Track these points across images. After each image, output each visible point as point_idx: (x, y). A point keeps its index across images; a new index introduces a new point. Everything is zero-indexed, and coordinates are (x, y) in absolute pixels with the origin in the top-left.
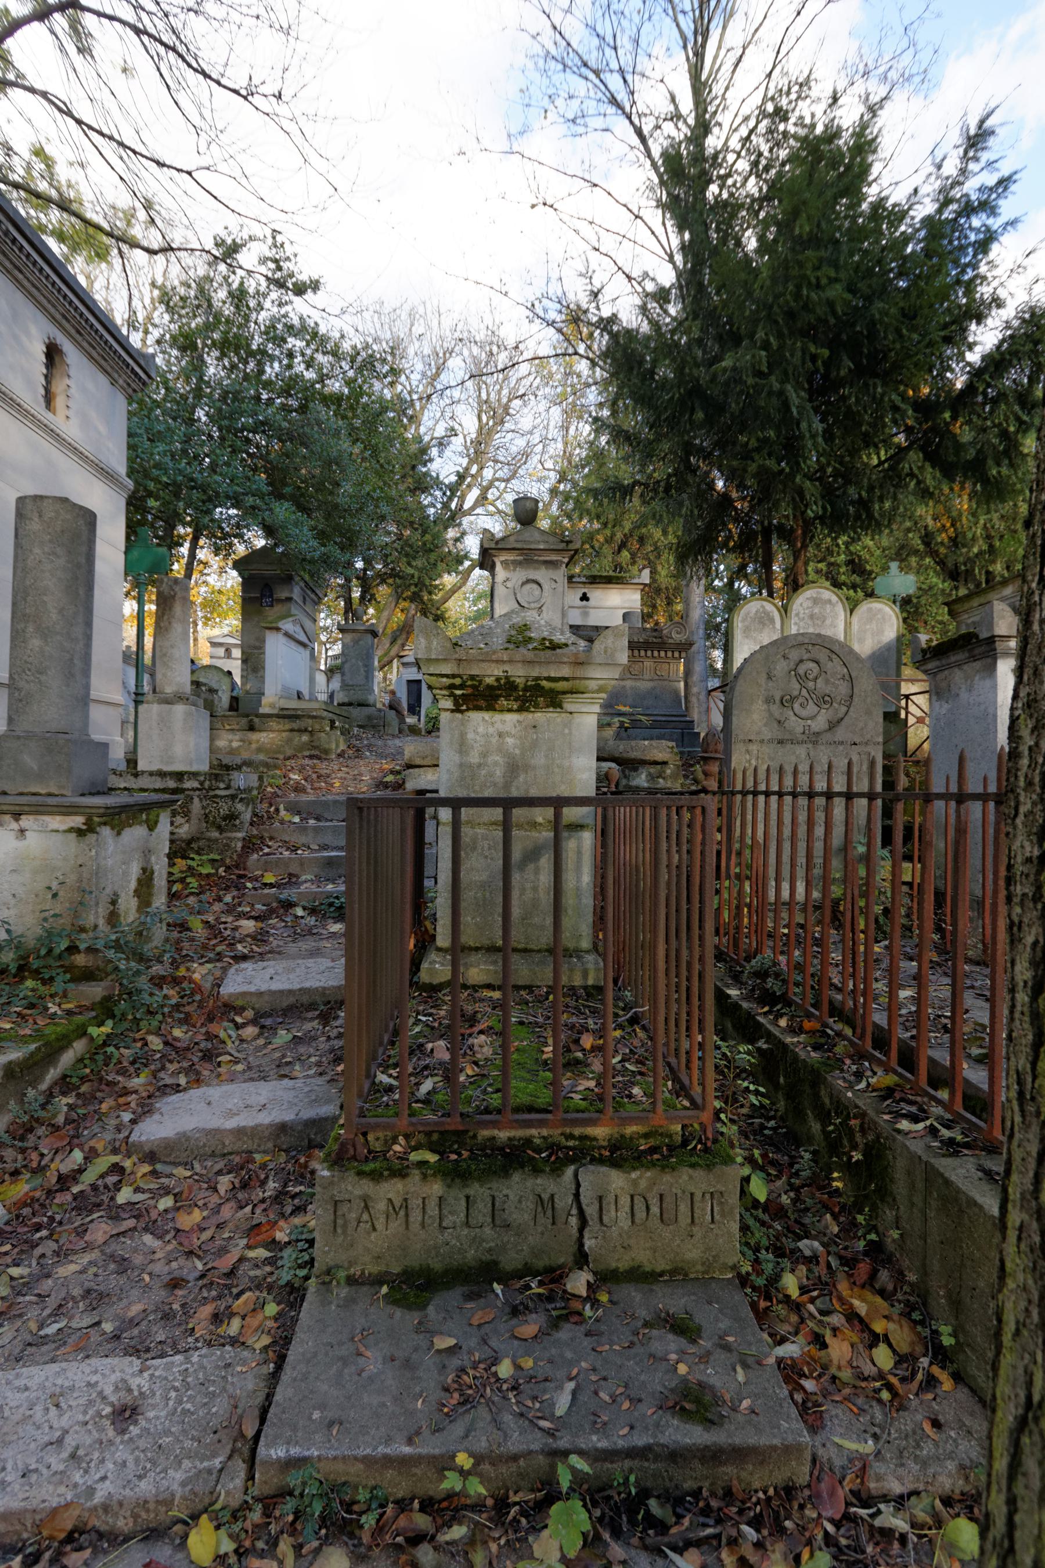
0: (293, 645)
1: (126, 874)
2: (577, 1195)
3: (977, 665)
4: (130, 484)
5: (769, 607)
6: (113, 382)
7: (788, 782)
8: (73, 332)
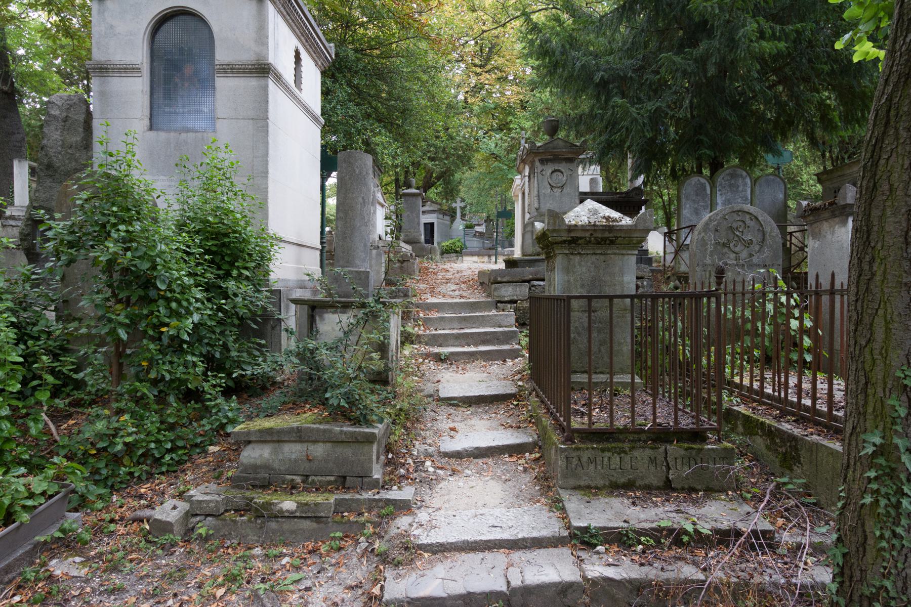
2: (666, 458)
3: (837, 220)
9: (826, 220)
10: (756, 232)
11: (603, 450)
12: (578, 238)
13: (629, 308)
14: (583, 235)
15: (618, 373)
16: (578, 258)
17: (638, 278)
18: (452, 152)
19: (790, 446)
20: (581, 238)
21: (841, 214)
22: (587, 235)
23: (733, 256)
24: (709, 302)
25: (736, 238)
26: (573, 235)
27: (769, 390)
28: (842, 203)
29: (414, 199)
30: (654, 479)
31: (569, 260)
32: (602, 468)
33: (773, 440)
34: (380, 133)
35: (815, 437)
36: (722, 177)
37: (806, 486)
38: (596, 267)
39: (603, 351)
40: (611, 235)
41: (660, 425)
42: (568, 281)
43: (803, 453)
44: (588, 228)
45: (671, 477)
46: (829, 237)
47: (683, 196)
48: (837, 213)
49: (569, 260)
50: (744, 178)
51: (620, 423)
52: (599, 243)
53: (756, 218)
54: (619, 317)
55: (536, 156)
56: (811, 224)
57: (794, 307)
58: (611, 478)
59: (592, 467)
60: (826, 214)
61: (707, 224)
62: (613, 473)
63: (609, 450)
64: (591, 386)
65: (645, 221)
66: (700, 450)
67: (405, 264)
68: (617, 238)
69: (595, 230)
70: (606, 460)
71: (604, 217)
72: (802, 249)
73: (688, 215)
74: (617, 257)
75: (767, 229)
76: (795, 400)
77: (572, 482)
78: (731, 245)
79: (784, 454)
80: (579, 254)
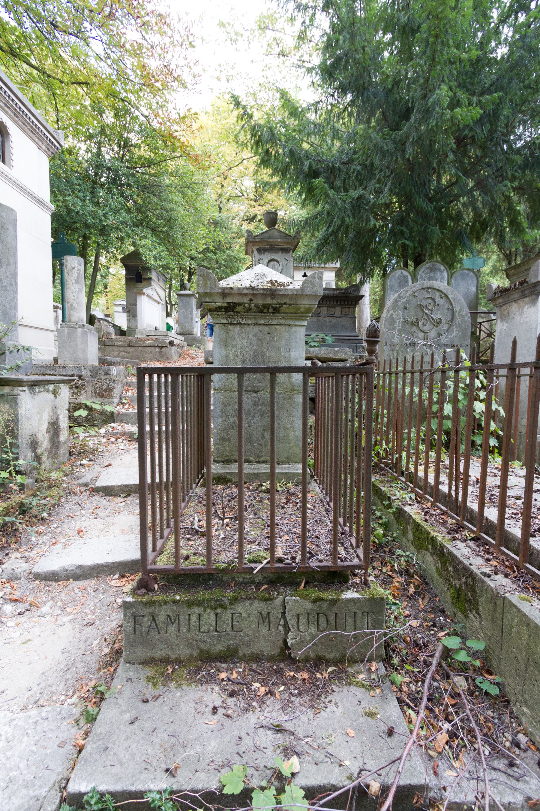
0: (152, 302)
1: (40, 419)
2: (284, 613)
3: (526, 300)
4: (53, 207)
5: (405, 273)
6: (40, 148)
7: (409, 367)
8: (12, 115)
9: (515, 301)
10: (445, 311)
11: (190, 604)
12: (235, 305)
13: (301, 389)
14: (241, 301)
15: (284, 462)
16: (237, 329)
18: (223, 262)
19: (466, 583)
20: (239, 304)
21: (532, 293)
22: (246, 300)
23: (421, 335)
24: (151, 377)
25: (425, 317)
26: (229, 300)
27: (444, 488)
28: (533, 281)
29: (188, 298)
30: (267, 646)
32: (189, 630)
33: (444, 564)
34: (145, 237)
35: (500, 579)
36: (422, 270)
37: (485, 656)
38: (258, 340)
40: (274, 301)
41: (281, 560)
42: (227, 356)
43: (482, 600)
44: (245, 291)
45: (290, 642)
46: (517, 318)
47: (387, 287)
48: (527, 292)
50: (442, 272)
51: (225, 557)
52: (261, 311)
53: (446, 296)
54: (285, 399)
55: (253, 245)
56: (501, 307)
57: (479, 389)
58: (202, 645)
59: (172, 629)
60: (516, 295)
61: (396, 301)
62: (205, 638)
63: (199, 604)
64: (240, 481)
65: (313, 285)
66: (334, 602)
67: (164, 349)
68: (281, 305)
69: (254, 295)
70: (194, 618)
71: (271, 282)
72: (490, 335)
74: (283, 329)
75: (457, 308)
76: (475, 507)
77: (141, 653)
78: (420, 324)
79: (459, 590)
80: (240, 324)
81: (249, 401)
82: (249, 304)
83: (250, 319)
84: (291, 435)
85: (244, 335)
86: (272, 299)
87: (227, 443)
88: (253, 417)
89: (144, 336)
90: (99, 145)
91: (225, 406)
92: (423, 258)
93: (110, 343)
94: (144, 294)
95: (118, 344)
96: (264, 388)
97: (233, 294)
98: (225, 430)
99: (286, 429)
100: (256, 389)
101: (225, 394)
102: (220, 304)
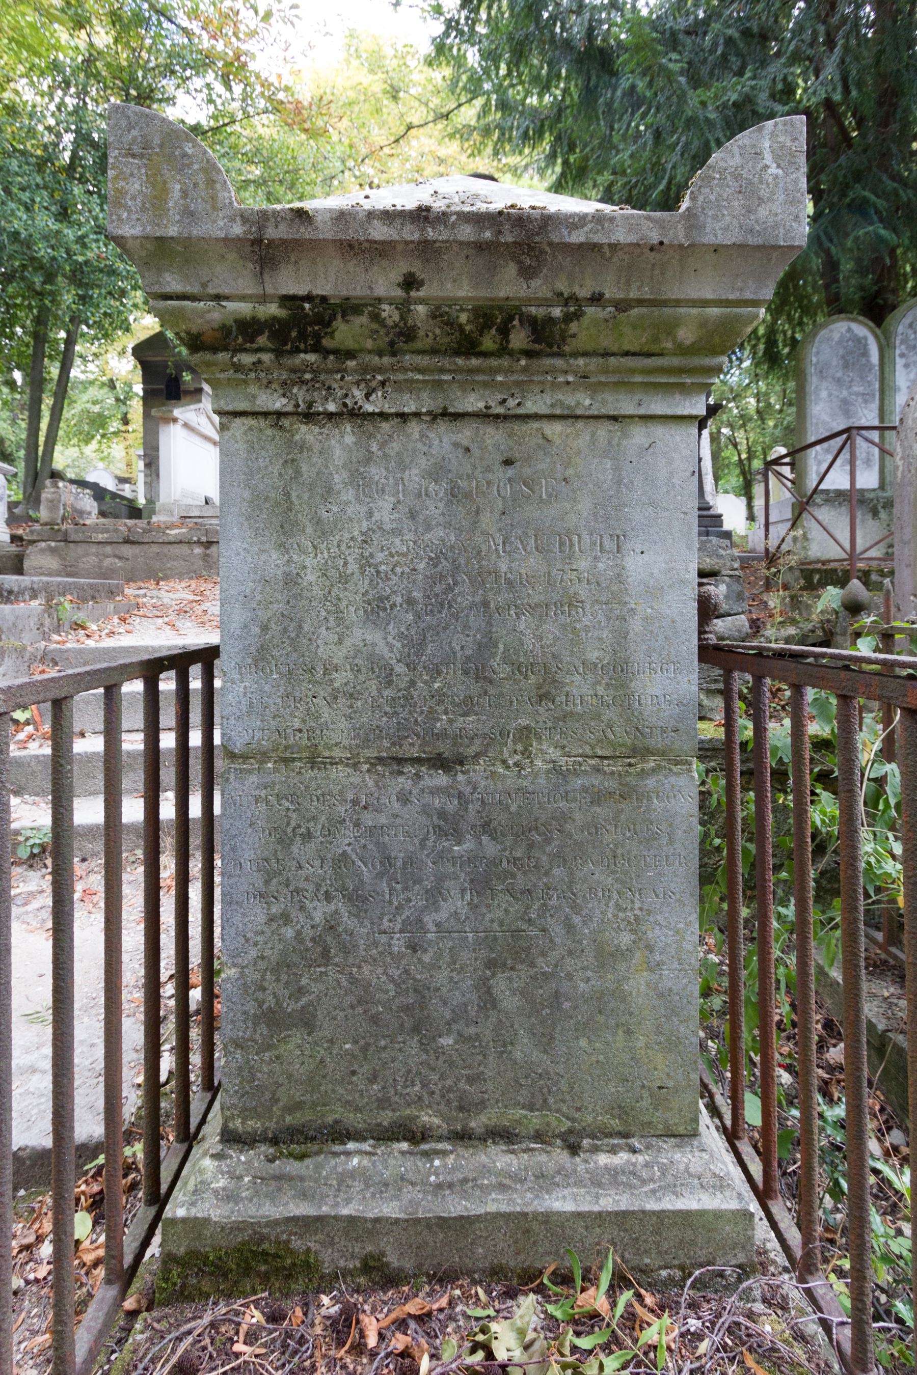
0: (197, 440)
14: (358, 290)
16: (346, 437)
17: (702, 574)
20: (349, 308)
22: (383, 283)
26: (291, 281)
31: (292, 457)
36: (907, 321)
38: (454, 494)
39: (510, 1002)
40: (539, 287)
42: (291, 581)
44: (379, 232)
49: (292, 457)
52: (467, 346)
54: (598, 797)
68: (574, 307)
69: (426, 250)
73: (826, 418)
74: (581, 437)
80: (355, 414)
81: (410, 813)
82: (404, 307)
83: (409, 386)
84: (638, 985)
85: (376, 472)
86: (527, 273)
87: (297, 1036)
88: (435, 896)
89: (175, 519)
90: (83, 93)
91: (284, 842)
92: (891, 298)
93: (80, 537)
94: (175, 420)
95: (101, 537)
96: (489, 741)
97: (315, 245)
98: (281, 966)
99: (608, 957)
100: (445, 748)
101: (281, 778)
102: (244, 309)
